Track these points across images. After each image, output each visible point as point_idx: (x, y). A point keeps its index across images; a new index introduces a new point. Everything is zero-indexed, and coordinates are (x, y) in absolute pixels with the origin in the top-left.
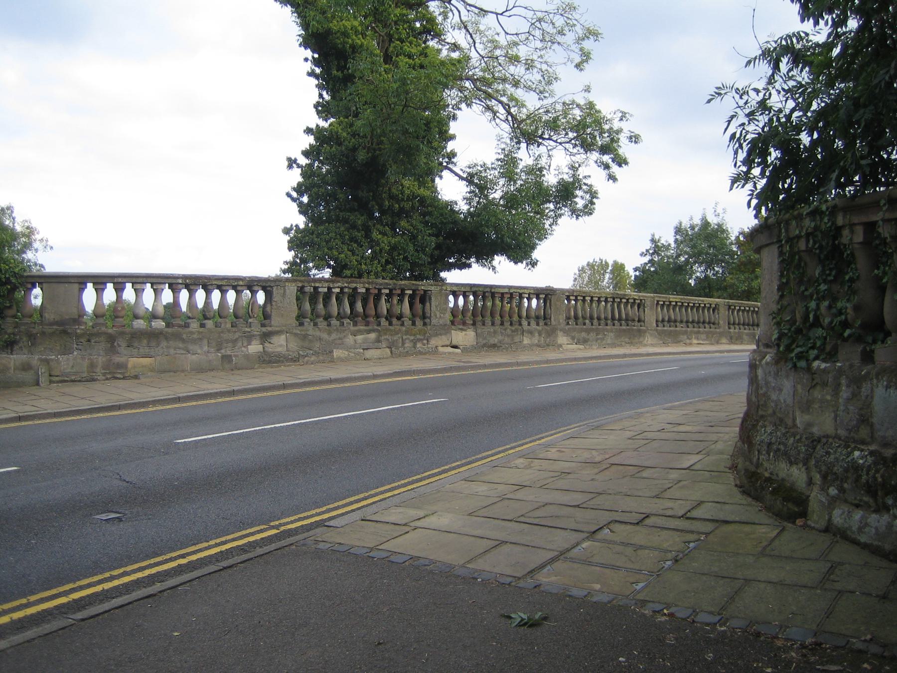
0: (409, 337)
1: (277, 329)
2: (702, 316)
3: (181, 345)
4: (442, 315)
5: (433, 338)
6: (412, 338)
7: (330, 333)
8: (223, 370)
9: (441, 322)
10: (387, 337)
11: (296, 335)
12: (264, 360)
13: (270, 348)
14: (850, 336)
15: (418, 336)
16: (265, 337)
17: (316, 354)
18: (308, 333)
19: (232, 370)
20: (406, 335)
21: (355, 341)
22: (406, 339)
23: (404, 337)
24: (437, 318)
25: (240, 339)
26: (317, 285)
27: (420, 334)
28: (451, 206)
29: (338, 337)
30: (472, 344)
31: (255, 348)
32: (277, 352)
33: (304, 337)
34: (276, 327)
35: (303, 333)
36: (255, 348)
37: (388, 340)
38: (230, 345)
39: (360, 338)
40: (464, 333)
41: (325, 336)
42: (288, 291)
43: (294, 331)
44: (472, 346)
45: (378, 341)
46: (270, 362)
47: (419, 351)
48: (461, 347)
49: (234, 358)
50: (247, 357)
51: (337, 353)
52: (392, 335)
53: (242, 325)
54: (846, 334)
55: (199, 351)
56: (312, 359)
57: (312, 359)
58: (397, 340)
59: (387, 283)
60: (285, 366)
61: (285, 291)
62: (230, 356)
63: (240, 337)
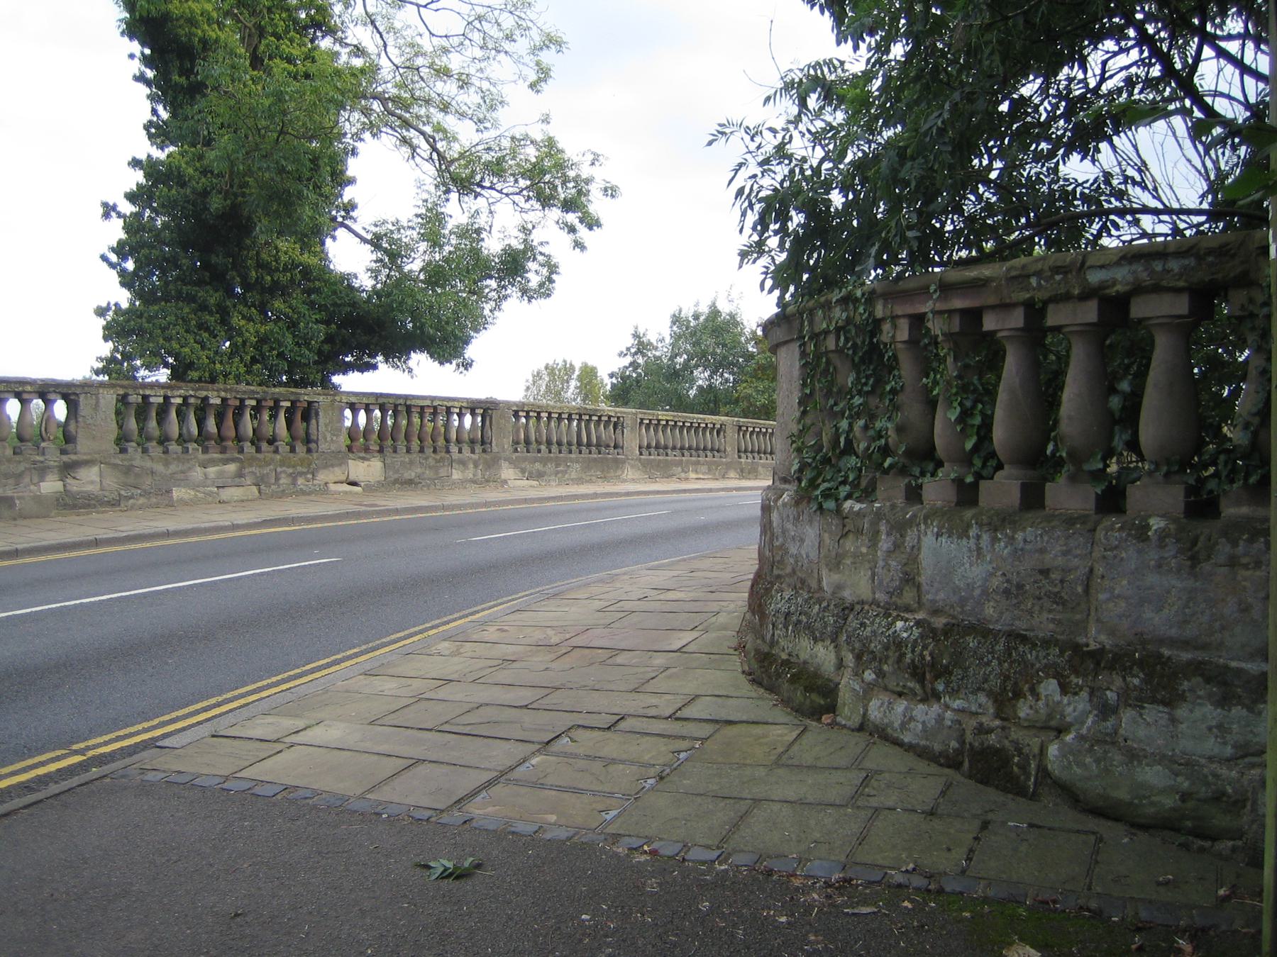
1: (85, 457)
6: (291, 470)
7: (167, 464)
11: (115, 466)
13: (74, 486)
15: (299, 469)
16: (67, 469)
17: (146, 494)
18: (134, 463)
19: (15, 519)
20: (281, 466)
23: (279, 469)
26: (148, 392)
27: (301, 466)
31: (51, 485)
33: (128, 470)
34: (85, 454)
35: (126, 463)
36: (51, 485)
37: (255, 474)
38: (11, 481)
39: (212, 470)
40: (367, 463)
41: (159, 468)
42: (102, 401)
43: (114, 461)
45: (240, 475)
46: (74, 507)
48: (362, 484)
49: (17, 502)
50: (39, 499)
51: (177, 493)
60: (98, 512)
62: (12, 498)
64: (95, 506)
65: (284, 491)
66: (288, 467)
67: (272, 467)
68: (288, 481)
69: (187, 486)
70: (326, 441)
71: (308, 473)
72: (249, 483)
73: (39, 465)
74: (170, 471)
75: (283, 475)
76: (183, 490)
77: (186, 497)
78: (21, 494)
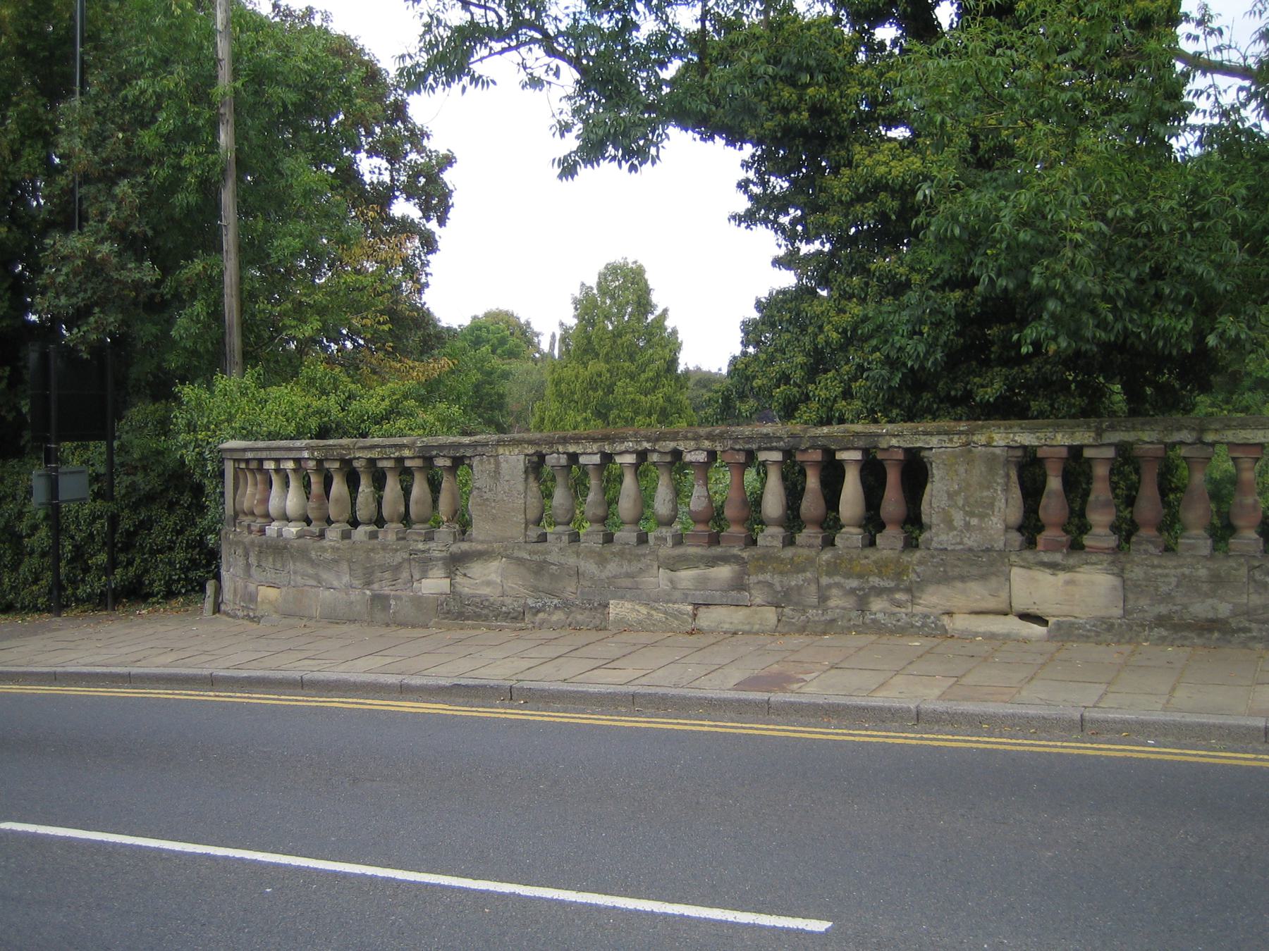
0: (842, 580)
1: (480, 547)
2: (623, 448)
3: (310, 571)
4: (974, 521)
5: (931, 588)
6: (854, 583)
7: (602, 561)
8: (371, 623)
9: (971, 541)
10: (768, 577)
11: (520, 561)
12: (449, 612)
13: (466, 586)
14: (1107, 426)
15: (875, 581)
16: (455, 562)
17: (566, 606)
18: (549, 558)
19: (388, 625)
20: (829, 574)
21: (672, 582)
22: (829, 586)
23: (825, 580)
24: (954, 528)
25: (406, 565)
26: (572, 449)
27: (880, 575)
28: (359, 120)
29: (624, 570)
30: (1103, 613)
31: (434, 584)
32: (480, 596)
33: (540, 568)
34: (482, 542)
35: (535, 557)
36: (434, 584)
37: (770, 585)
38: (387, 575)
39: (687, 576)
40: (1062, 576)
41: (589, 567)
42: (504, 465)
43: (517, 553)
44: (1103, 620)
45: (739, 585)
46: (461, 616)
47: (874, 621)
48: (1052, 621)
49: (393, 602)
50: (418, 601)
51: (618, 609)
52: (781, 573)
53: (416, 537)
54: (1104, 426)
55: (336, 584)
56: (555, 618)
57: (555, 618)
58: (799, 588)
59: (767, 435)
60: (489, 628)
61: (498, 465)
62: (387, 597)
63: (404, 560)
64: (486, 618)
65: (833, 621)
66: (848, 576)
67: (808, 575)
68: (849, 602)
69: (637, 599)
70: (951, 527)
71: (897, 589)
72: (758, 600)
73: (420, 555)
74: (606, 573)
75: (834, 591)
76: (628, 605)
77: (632, 616)
78: (399, 593)
